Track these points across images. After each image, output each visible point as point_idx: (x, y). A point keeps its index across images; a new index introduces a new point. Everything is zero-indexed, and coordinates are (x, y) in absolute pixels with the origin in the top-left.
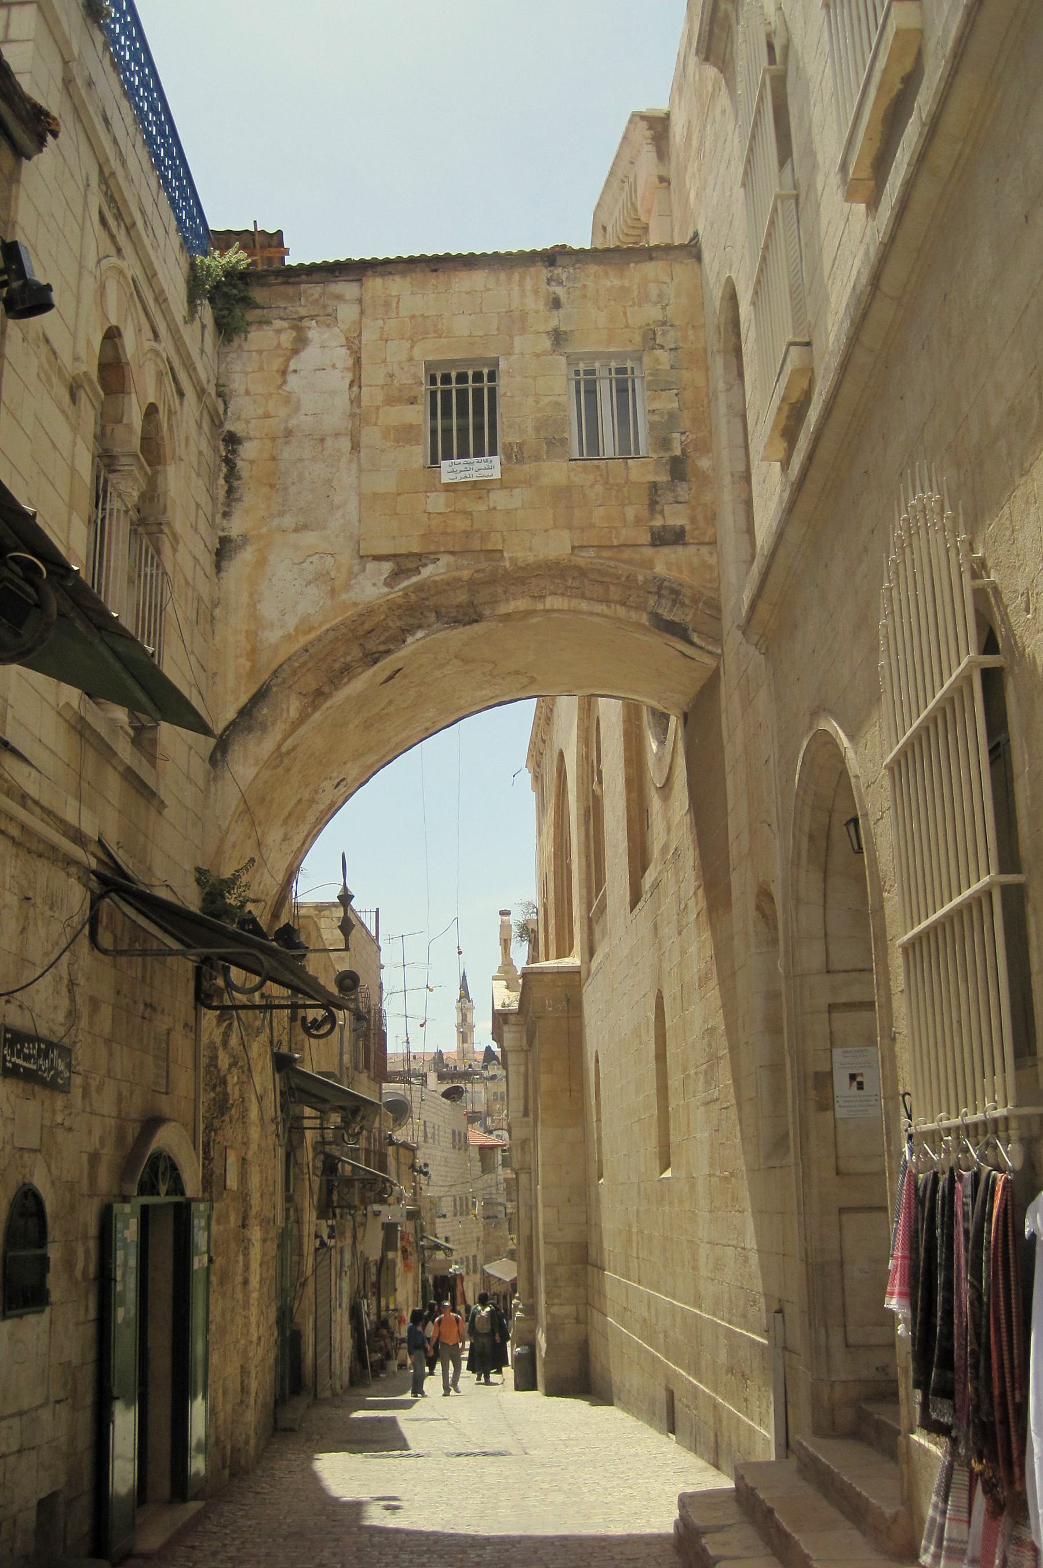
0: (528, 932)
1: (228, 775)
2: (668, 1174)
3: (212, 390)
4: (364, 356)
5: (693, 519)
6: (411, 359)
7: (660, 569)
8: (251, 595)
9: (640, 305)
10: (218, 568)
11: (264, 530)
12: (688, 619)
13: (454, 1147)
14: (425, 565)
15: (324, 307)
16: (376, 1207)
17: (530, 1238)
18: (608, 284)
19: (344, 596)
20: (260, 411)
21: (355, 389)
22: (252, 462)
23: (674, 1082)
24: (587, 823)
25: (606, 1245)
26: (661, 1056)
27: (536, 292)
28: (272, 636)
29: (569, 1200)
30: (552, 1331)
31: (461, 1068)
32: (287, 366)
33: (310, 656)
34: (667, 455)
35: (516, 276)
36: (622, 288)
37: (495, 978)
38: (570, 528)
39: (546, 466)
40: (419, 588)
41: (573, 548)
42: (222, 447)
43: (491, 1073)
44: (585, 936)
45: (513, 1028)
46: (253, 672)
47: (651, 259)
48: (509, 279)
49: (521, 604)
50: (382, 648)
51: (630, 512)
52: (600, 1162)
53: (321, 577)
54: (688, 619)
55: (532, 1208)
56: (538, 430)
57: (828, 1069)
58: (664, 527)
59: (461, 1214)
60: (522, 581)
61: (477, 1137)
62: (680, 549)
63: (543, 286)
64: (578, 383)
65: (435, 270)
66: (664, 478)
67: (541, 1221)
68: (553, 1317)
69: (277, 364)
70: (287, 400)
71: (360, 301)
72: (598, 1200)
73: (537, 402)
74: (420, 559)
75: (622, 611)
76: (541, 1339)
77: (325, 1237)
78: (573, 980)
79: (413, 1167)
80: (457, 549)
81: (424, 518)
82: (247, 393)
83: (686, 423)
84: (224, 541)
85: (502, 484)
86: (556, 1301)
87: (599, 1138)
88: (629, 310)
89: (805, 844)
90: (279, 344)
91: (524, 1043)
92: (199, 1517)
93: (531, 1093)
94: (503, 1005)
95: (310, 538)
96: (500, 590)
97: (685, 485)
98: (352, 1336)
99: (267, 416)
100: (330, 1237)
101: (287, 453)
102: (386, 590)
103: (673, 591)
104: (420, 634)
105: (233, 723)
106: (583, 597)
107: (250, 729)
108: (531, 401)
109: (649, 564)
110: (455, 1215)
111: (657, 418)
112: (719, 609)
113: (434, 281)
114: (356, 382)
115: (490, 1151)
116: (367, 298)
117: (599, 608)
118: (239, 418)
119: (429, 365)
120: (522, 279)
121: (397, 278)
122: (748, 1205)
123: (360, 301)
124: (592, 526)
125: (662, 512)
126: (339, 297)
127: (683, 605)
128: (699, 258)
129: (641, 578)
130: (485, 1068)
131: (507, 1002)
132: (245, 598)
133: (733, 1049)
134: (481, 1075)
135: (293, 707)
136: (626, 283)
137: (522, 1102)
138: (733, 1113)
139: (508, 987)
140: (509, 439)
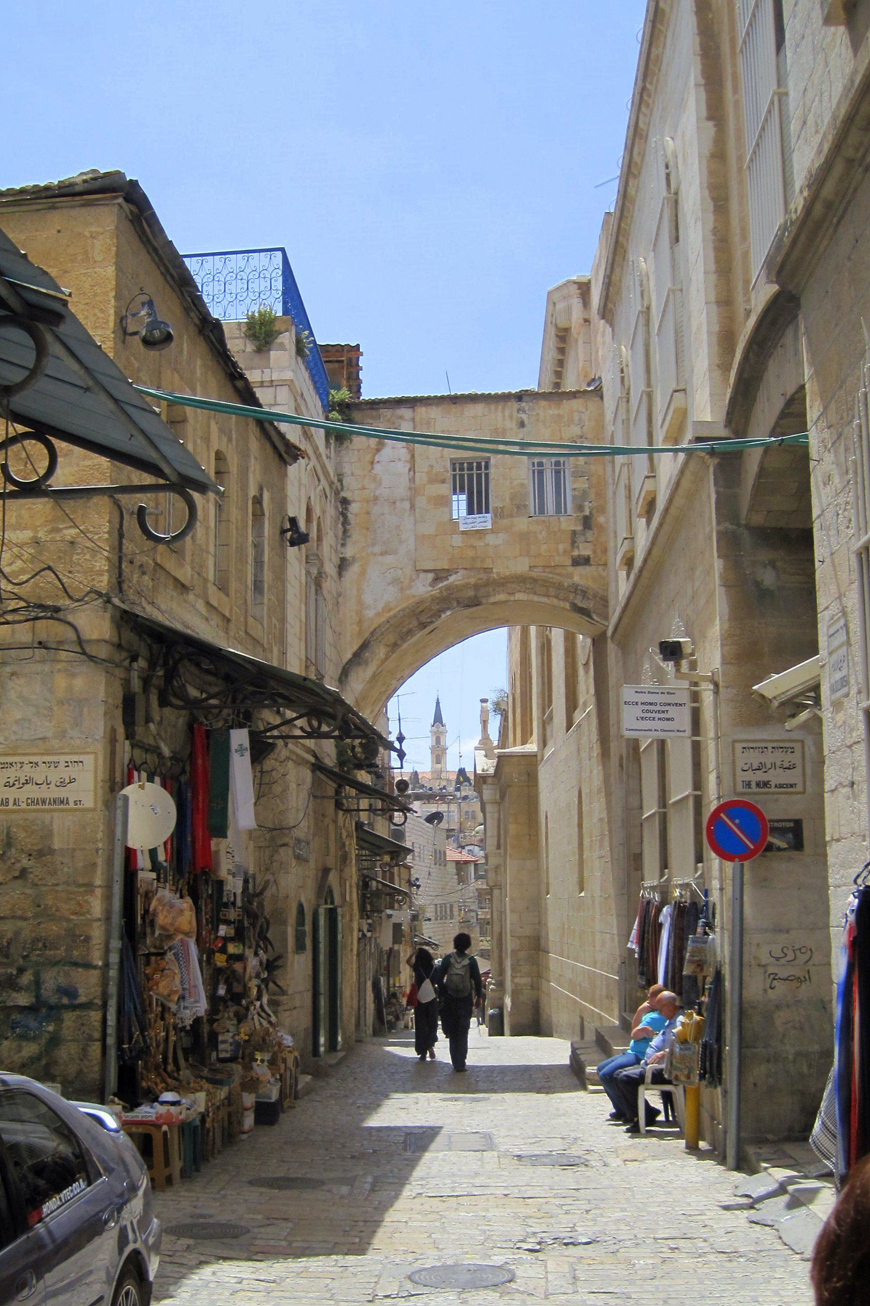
0: (498, 708)
1: (348, 688)
2: (582, 894)
3: (336, 481)
4: (416, 454)
5: (594, 552)
6: (442, 457)
7: (576, 579)
8: (358, 590)
9: (569, 426)
10: (340, 575)
11: (364, 554)
12: (591, 606)
13: (435, 864)
14: (451, 575)
15: (393, 423)
16: (389, 912)
17: (500, 934)
18: (551, 412)
19: (408, 592)
20: (360, 486)
21: (412, 473)
22: (356, 515)
23: (586, 842)
24: (543, 654)
25: (551, 938)
26: (580, 825)
27: (511, 417)
28: (370, 613)
29: (528, 908)
30: (515, 995)
31: (436, 787)
32: (373, 460)
33: (391, 625)
34: (581, 514)
35: (500, 407)
36: (559, 415)
37: (476, 749)
38: (528, 556)
39: (516, 520)
40: (448, 588)
41: (530, 567)
42: (339, 506)
43: (463, 794)
44: (541, 731)
45: (490, 787)
46: (360, 633)
47: (575, 397)
48: (496, 409)
49: (501, 597)
50: (429, 620)
51: (561, 547)
52: (548, 883)
53: (396, 581)
54: (591, 606)
55: (502, 913)
56: (512, 499)
57: (639, 851)
58: (579, 556)
59: (441, 919)
60: (503, 584)
61: (453, 854)
62: (587, 567)
63: (515, 414)
64: (534, 471)
65: (455, 403)
66: (579, 528)
67: (508, 922)
68: (516, 984)
69: (368, 458)
70: (374, 479)
71: (413, 420)
72: (546, 909)
73: (511, 483)
74: (448, 572)
75: (555, 602)
76: (508, 1001)
77: (365, 931)
78: (531, 761)
79: (409, 881)
80: (468, 567)
81: (450, 549)
82: (353, 474)
83: (592, 496)
84: (343, 560)
85: (492, 531)
86: (518, 975)
87: (547, 868)
88: (563, 429)
89: (631, 752)
90: (369, 446)
91: (498, 797)
92: (344, 1059)
93: (502, 832)
94: (483, 770)
95: (389, 559)
96: (491, 589)
97: (591, 532)
98: (374, 1002)
99: (363, 488)
100: (369, 931)
101: (376, 510)
102: (431, 588)
103: (582, 591)
104: (448, 613)
105: (350, 661)
106: (535, 593)
107: (359, 664)
108: (508, 482)
109: (571, 576)
110: (436, 919)
111: (577, 493)
112: (607, 602)
113: (455, 409)
114: (412, 469)
115: (464, 866)
116: (417, 419)
117: (545, 600)
118: (348, 489)
119: (451, 460)
120: (503, 409)
121: (434, 408)
122: (614, 912)
123: (413, 420)
124: (540, 555)
125: (578, 547)
126: (401, 417)
127: (588, 598)
128: (602, 398)
129: (566, 584)
130: (458, 789)
131: (486, 768)
132: (355, 592)
133: (610, 831)
134: (454, 796)
135: (381, 652)
136: (561, 412)
137: (495, 839)
138: (609, 865)
139: (486, 756)
140: (496, 505)
